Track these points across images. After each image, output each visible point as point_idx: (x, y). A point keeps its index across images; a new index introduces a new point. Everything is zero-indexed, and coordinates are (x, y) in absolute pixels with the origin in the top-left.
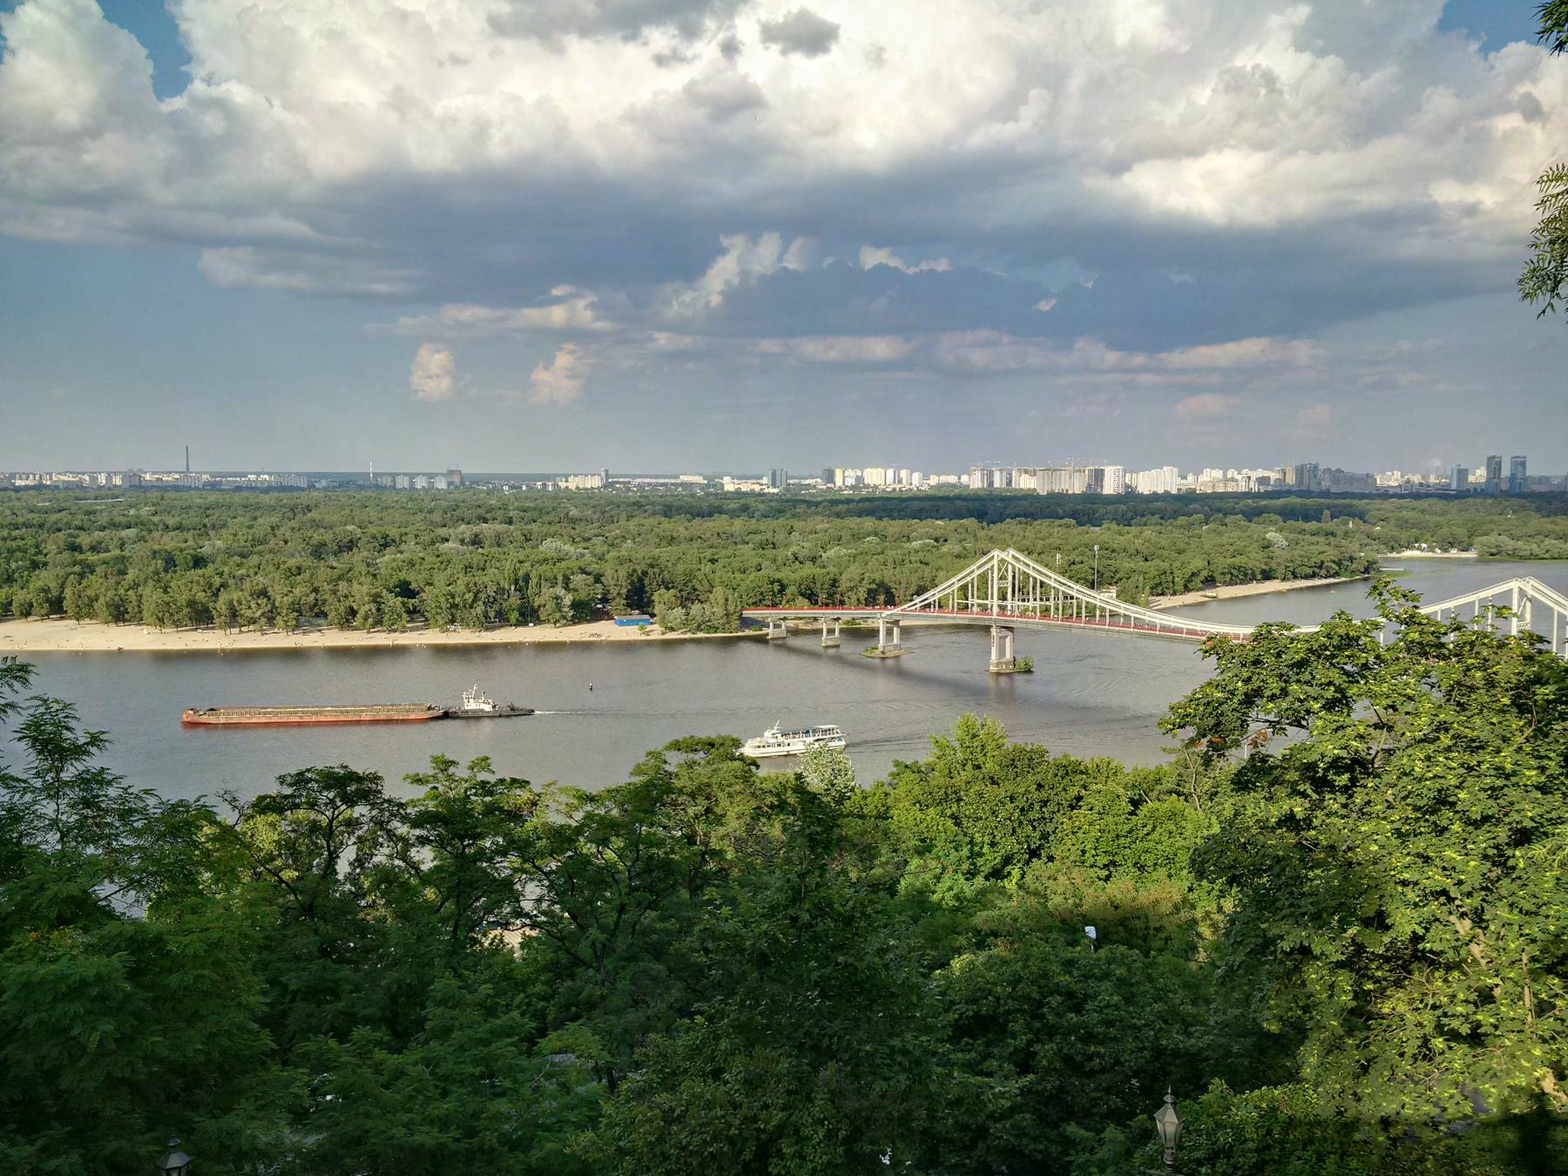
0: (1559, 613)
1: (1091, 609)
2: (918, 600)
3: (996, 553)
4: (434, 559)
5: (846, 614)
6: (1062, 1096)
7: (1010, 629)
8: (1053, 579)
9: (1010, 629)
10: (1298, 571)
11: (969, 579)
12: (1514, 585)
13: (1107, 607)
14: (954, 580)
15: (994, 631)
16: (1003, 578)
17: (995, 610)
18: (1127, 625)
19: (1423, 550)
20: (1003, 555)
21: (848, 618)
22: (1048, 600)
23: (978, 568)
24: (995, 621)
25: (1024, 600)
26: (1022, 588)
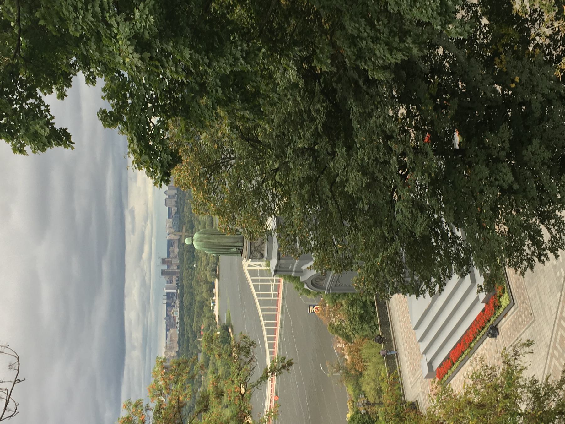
19: (215, 305)
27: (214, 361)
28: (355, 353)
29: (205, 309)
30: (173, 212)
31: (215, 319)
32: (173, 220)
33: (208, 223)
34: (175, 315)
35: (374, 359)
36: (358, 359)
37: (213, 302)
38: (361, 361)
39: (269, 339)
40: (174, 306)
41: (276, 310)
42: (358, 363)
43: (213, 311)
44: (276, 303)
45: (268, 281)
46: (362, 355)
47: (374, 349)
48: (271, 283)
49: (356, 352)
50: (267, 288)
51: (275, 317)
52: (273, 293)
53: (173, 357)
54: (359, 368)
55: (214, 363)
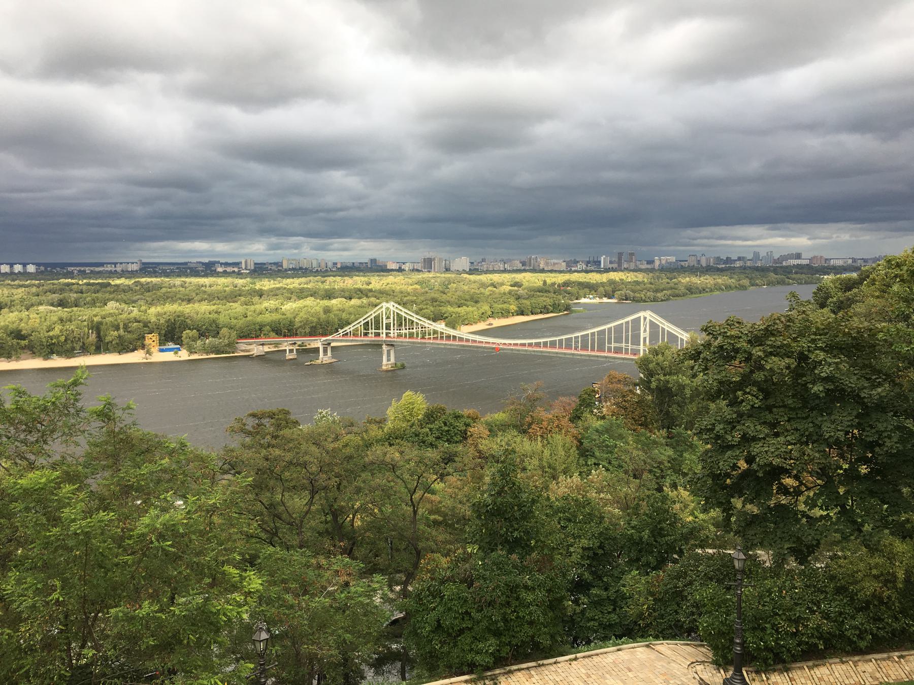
0: (667, 331)
1: (435, 332)
2: (341, 331)
3: (384, 305)
4: (35, 315)
5: (299, 340)
6: (286, 432)
7: (392, 345)
8: (415, 318)
9: (392, 345)
10: (533, 310)
11: (369, 319)
12: (642, 314)
13: (444, 332)
14: (361, 319)
15: (384, 347)
16: (388, 318)
17: (384, 335)
18: (442, 338)
19: (591, 299)
20: (388, 305)
21: (299, 343)
22: (413, 329)
23: (374, 313)
24: (385, 341)
25: (400, 330)
26: (401, 321)
27: (535, 296)
28: (556, 423)
29: (587, 290)
30: (683, 263)
31: (577, 299)
32: (674, 263)
33: (677, 292)
34: (579, 266)
35: (547, 453)
36: (546, 429)
37: (594, 298)
38: (544, 433)
39: (560, 341)
40: (587, 266)
41: (593, 350)
42: (541, 428)
43: (585, 298)
44: (601, 349)
45: (627, 342)
46: (554, 435)
47: (563, 453)
48: (624, 344)
49: (557, 426)
50: (618, 340)
51: (585, 347)
52: (613, 346)
53: (539, 266)
54: (534, 429)
55: (533, 296)
